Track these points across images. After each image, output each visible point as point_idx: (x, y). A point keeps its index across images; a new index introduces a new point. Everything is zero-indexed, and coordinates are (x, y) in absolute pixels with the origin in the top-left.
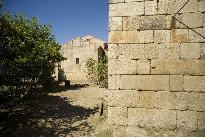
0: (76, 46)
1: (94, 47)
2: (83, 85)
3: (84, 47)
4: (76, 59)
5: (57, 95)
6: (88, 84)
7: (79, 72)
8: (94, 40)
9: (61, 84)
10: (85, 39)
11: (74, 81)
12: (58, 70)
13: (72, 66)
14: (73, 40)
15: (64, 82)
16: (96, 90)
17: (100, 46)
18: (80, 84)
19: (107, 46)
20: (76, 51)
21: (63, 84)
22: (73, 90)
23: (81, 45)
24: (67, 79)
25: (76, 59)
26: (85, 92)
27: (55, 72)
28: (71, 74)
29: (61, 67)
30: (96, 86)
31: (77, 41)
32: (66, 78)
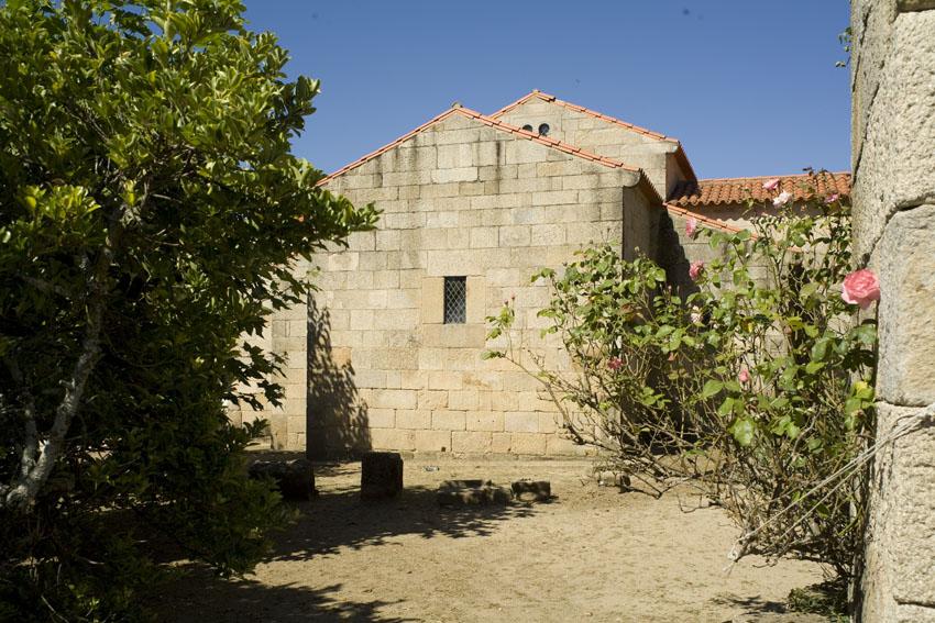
0: (439, 177)
1: (586, 182)
2: (507, 487)
3: (505, 187)
4: (446, 285)
5: (297, 577)
6: (546, 486)
7: (468, 382)
8: (582, 127)
9: (324, 483)
10: (514, 118)
11: (428, 454)
12: (310, 375)
13: (412, 340)
14: (420, 136)
15: (356, 460)
16: (620, 535)
17: (641, 171)
18: (479, 483)
19: (683, 178)
20: (446, 220)
21: (346, 479)
22: (428, 535)
23: (479, 167)
24: (379, 444)
25: (447, 278)
26: (527, 558)
27: (276, 386)
28: (404, 400)
29: (328, 348)
30: (610, 502)
31: (454, 137)
32: (368, 436)
